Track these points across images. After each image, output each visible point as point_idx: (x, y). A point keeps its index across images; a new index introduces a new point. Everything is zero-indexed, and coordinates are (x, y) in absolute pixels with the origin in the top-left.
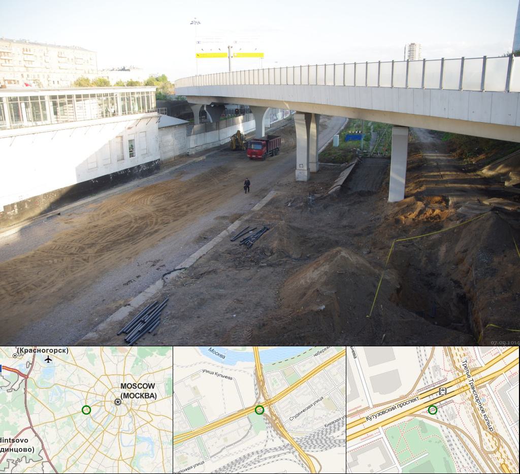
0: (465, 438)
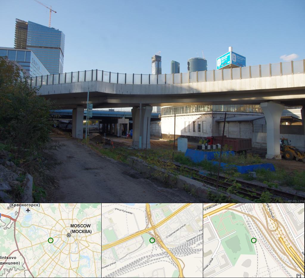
0: (258, 223)
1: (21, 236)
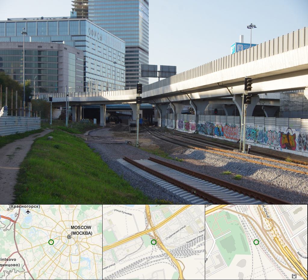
0: (253, 222)
1: (21, 237)
